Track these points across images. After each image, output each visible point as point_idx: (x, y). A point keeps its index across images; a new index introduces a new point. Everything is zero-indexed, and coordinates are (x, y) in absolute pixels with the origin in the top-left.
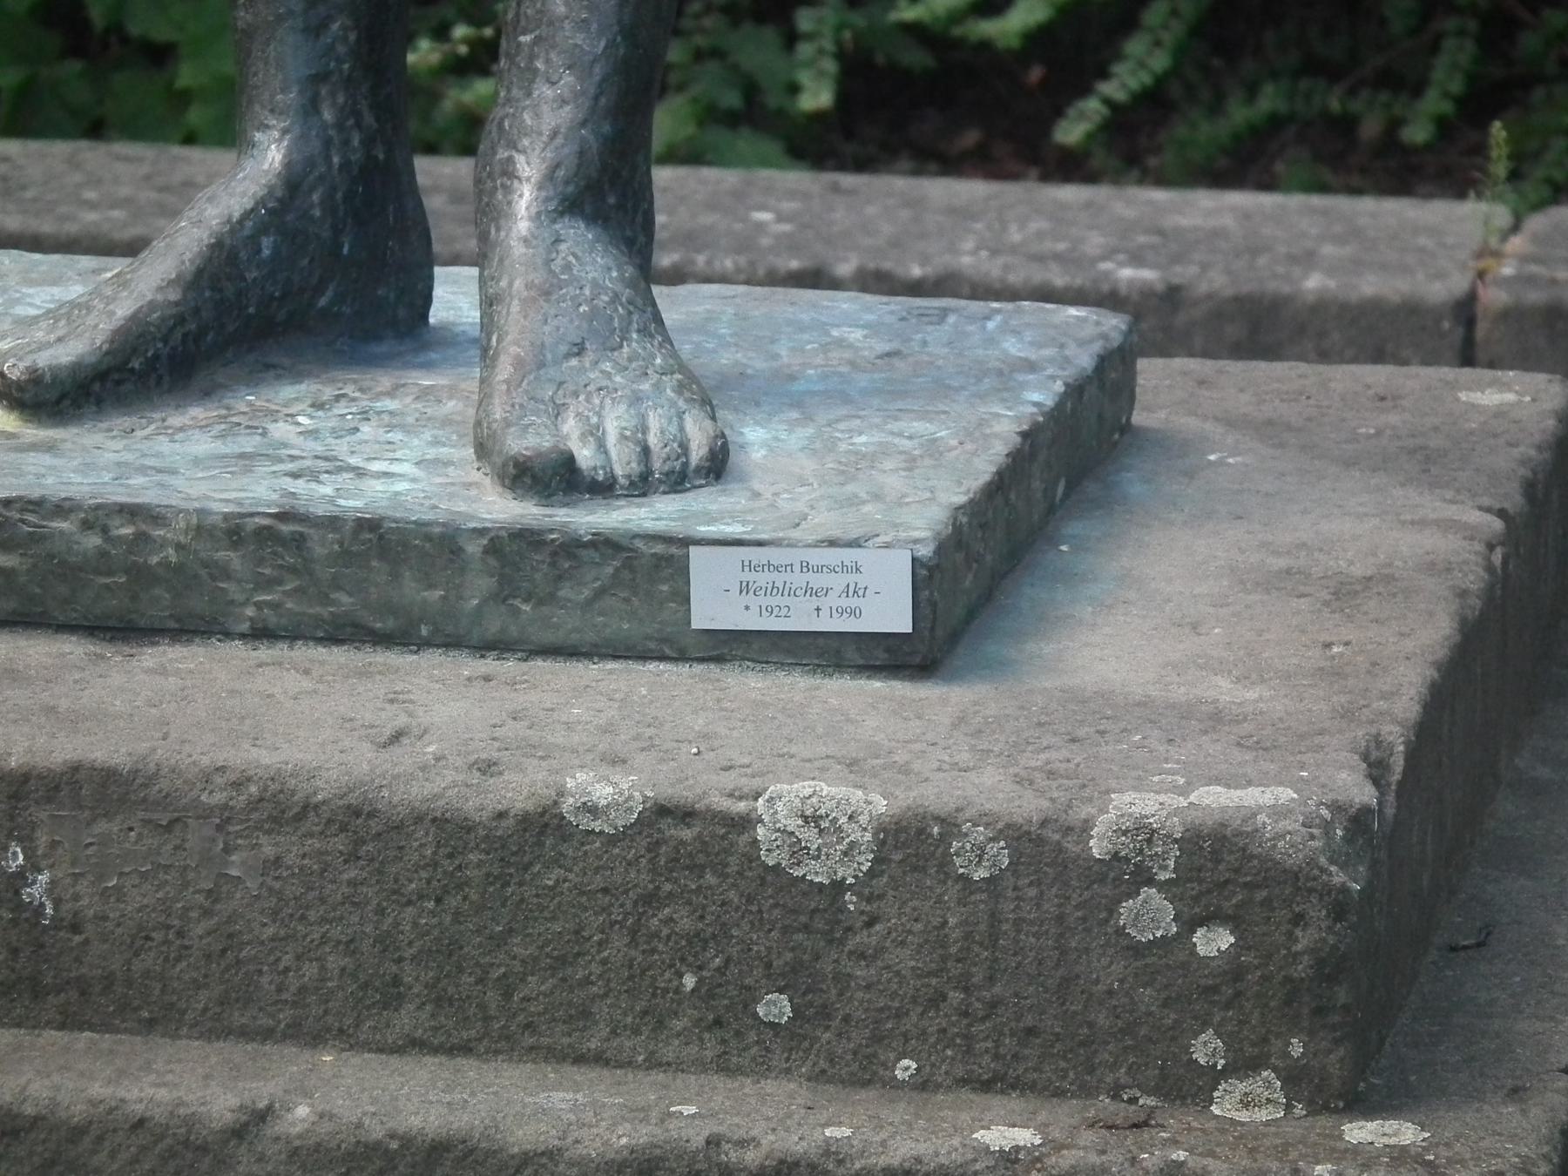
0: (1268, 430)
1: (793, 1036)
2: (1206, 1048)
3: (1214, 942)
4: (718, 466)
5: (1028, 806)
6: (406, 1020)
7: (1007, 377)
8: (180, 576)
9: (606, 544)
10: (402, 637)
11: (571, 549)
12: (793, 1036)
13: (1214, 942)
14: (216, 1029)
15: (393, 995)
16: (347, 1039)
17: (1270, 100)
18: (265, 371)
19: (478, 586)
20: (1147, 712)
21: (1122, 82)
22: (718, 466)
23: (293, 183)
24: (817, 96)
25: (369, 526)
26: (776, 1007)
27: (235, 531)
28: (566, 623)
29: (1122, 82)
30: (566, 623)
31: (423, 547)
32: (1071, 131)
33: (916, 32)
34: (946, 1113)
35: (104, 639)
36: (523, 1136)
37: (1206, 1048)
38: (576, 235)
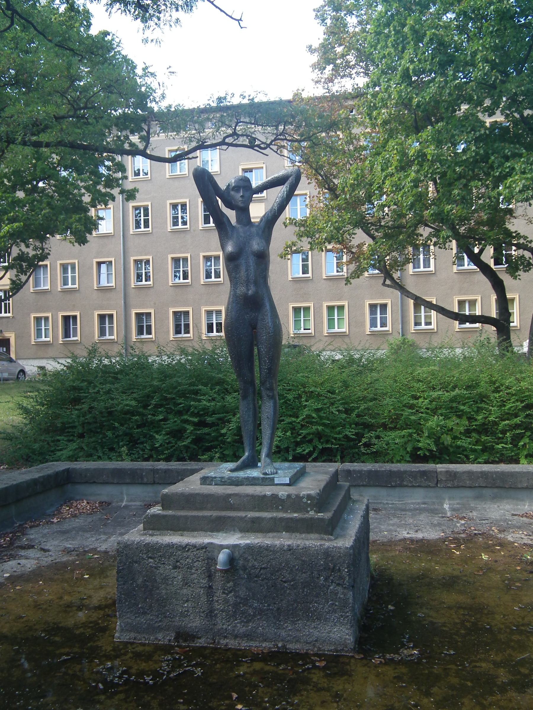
0: (315, 472)
1: (282, 509)
2: (309, 509)
3: (309, 502)
5: (296, 493)
6: (256, 509)
8: (241, 481)
9: (269, 478)
10: (256, 485)
12: (282, 509)
13: (309, 502)
15: (255, 508)
16: (252, 511)
17: (325, 458)
18: (247, 469)
19: (261, 481)
21: (313, 456)
22: (276, 473)
23: (248, 456)
26: (280, 507)
28: (266, 483)
29: (313, 456)
30: (266, 483)
32: (309, 460)
35: (211, 459)
36: (264, 516)
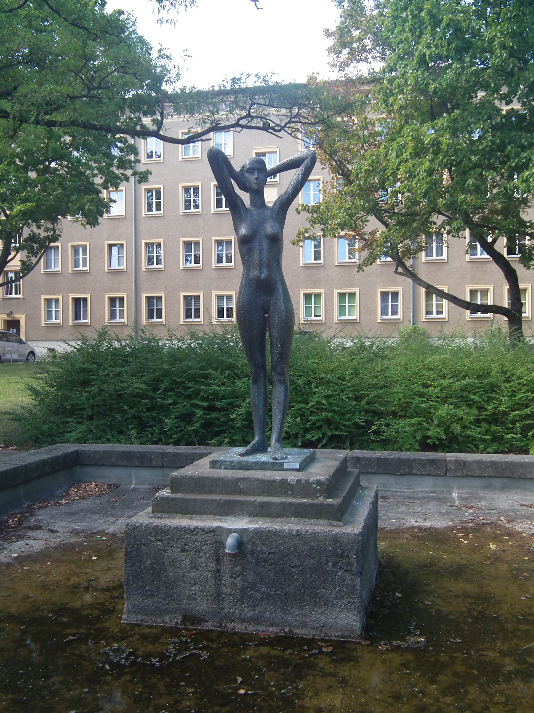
0: (325, 458)
1: (291, 495)
2: (318, 495)
3: (318, 487)
4: (286, 458)
5: (306, 479)
7: (306, 453)
10: (265, 469)
11: (276, 463)
12: (291, 495)
13: (318, 487)
14: (253, 495)
15: (264, 492)
17: (334, 445)
19: (270, 466)
20: (314, 473)
22: (286, 458)
23: (258, 441)
24: (300, 444)
25: (263, 462)
26: (290, 493)
27: (254, 463)
28: (276, 468)
29: (323, 443)
30: (276, 468)
31: (150, 95)
32: (319, 447)
33: (307, 440)
34: (123, 127)
36: (273, 501)
37: (318, 495)
38: (277, 443)
